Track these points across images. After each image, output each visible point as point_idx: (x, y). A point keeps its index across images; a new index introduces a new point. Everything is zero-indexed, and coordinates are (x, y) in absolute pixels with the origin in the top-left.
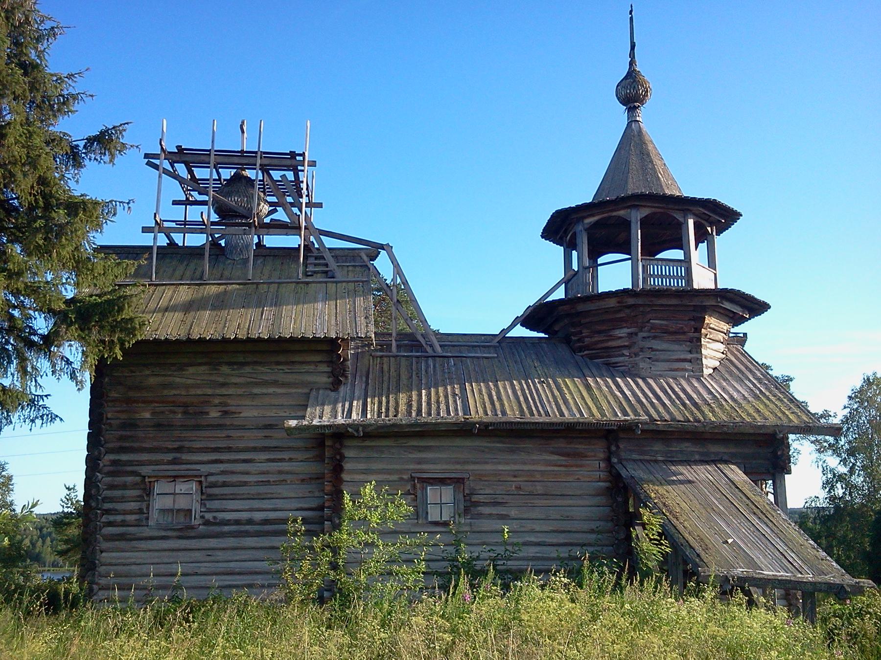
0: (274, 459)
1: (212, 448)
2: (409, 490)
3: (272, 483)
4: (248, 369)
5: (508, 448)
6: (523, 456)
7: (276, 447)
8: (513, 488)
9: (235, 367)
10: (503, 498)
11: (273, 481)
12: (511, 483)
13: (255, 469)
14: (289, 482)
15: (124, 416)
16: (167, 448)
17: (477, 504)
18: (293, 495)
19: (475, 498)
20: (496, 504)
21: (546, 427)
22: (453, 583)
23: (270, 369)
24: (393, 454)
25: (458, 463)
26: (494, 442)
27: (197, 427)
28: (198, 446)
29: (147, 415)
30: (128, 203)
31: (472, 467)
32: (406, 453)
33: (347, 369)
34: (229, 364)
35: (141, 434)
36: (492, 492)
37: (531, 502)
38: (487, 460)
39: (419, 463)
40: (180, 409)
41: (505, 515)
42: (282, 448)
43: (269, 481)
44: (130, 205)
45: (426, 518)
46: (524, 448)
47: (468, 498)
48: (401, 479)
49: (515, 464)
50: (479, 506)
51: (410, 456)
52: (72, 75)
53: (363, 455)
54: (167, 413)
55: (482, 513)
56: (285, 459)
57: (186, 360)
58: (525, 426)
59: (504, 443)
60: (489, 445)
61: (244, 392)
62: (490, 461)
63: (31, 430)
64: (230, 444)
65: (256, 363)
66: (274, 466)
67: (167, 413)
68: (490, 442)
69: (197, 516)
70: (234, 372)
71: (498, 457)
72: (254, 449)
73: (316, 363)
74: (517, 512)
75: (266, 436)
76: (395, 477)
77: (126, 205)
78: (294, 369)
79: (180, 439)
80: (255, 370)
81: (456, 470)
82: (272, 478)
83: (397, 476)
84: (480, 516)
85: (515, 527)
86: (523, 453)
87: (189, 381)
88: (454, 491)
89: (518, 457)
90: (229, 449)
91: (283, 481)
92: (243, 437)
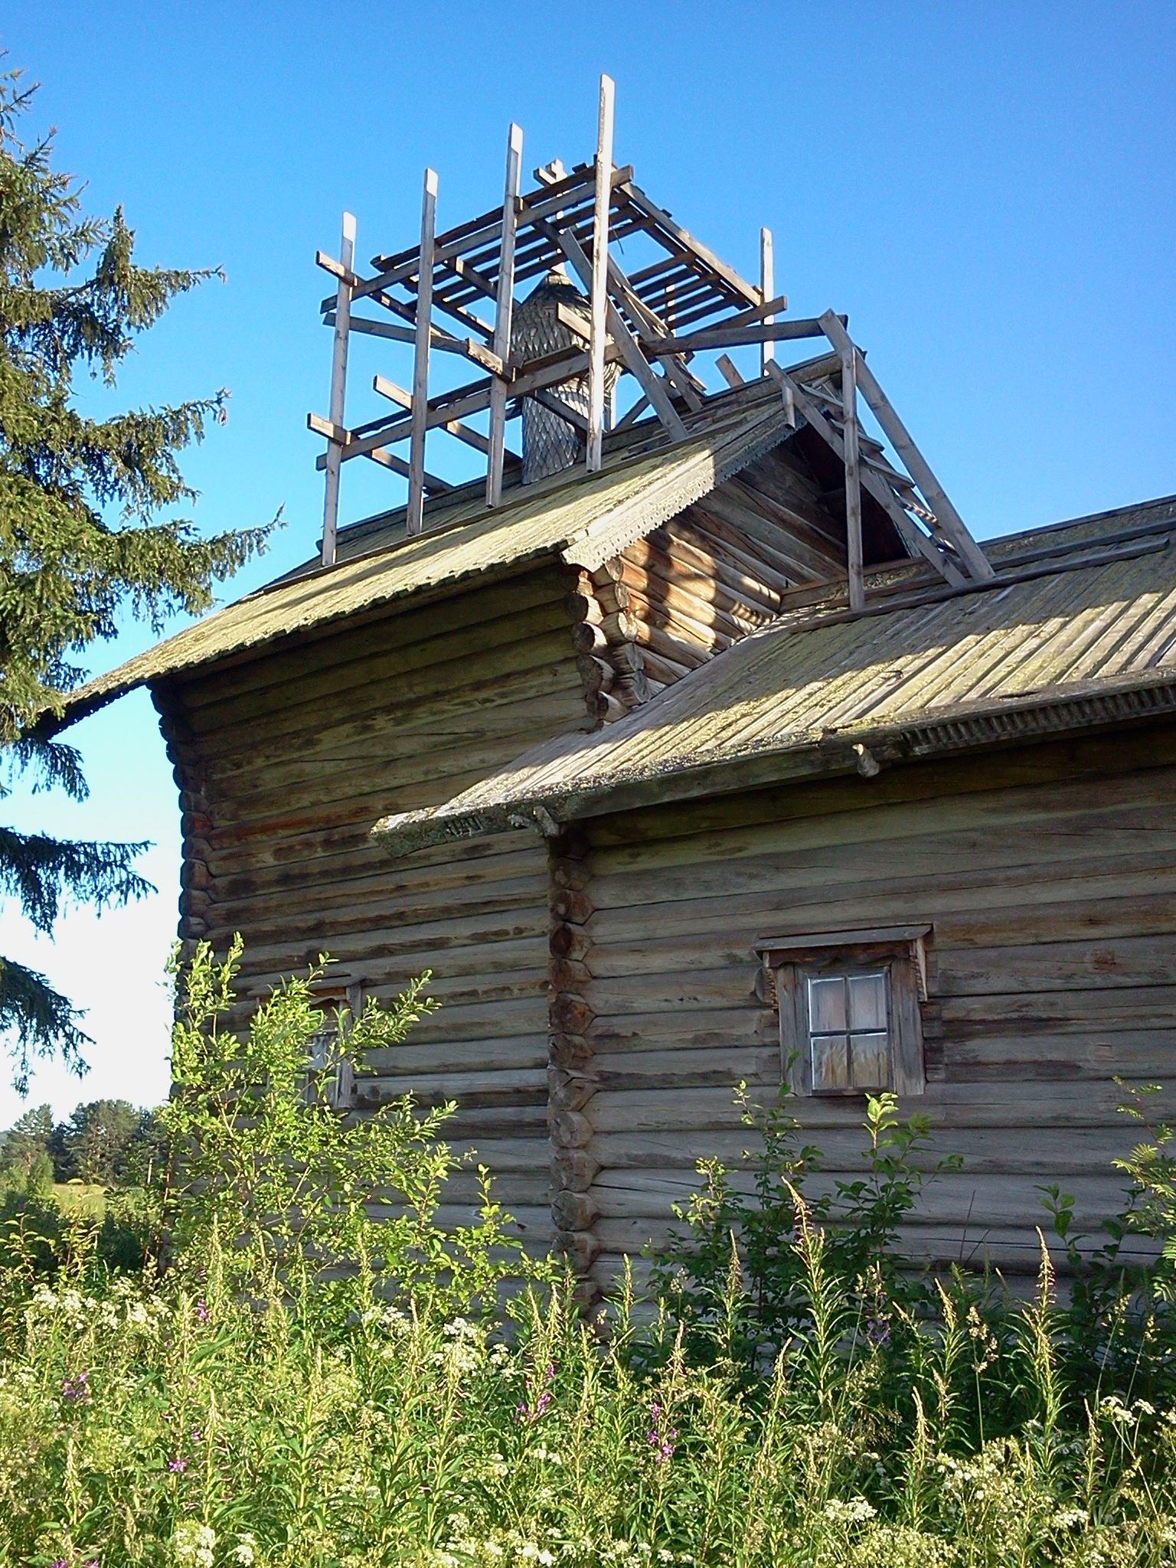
0: (486, 934)
1: (370, 920)
2: (754, 994)
3: (484, 998)
4: (423, 717)
5: (1066, 822)
6: (1120, 846)
7: (486, 904)
8: (1090, 967)
9: (399, 714)
10: (1052, 1004)
11: (485, 992)
12: (1076, 947)
13: (448, 962)
14: (516, 991)
15: (234, 867)
16: (297, 928)
17: (961, 1029)
18: (527, 1028)
19: (954, 1010)
20: (1031, 1025)
21: (1125, 712)
22: (945, 1300)
23: (464, 703)
24: (708, 885)
25: (894, 894)
26: (1009, 810)
27: (348, 873)
28: (347, 918)
29: (268, 859)
30: (219, 401)
31: (938, 904)
32: (741, 880)
33: (626, 666)
34: (388, 709)
35: (258, 903)
36: (1015, 986)
37: (1161, 1010)
38: (992, 875)
39: (778, 907)
40: (320, 837)
41: (1064, 1065)
42: (502, 903)
43: (474, 993)
44: (222, 405)
45: (805, 1080)
46: (1122, 814)
47: (932, 1010)
48: (734, 961)
49: (1091, 874)
50: (971, 1036)
51: (757, 886)
52: (33, 157)
53: (634, 897)
54: (298, 847)
55: (981, 1058)
56: (507, 933)
57: (312, 721)
58: (1043, 722)
59: (1047, 807)
60: (995, 821)
61: (426, 773)
62: (1002, 875)
63: (99, 915)
64: (398, 905)
65: (438, 695)
66: (483, 953)
67: (298, 847)
68: (994, 811)
69: (342, 1089)
70: (400, 728)
71: (1033, 859)
72: (448, 913)
73: (551, 667)
74: (1106, 1052)
75: (468, 878)
76: (712, 957)
77: (215, 406)
78: (513, 693)
79: (324, 905)
80: (435, 714)
81: (896, 917)
82: (480, 984)
83: (720, 953)
84: (972, 1069)
85: (1102, 1107)
86: (1118, 834)
87: (329, 768)
88: (890, 990)
89: (1099, 852)
90: (401, 919)
91: (504, 989)
92: (427, 884)
